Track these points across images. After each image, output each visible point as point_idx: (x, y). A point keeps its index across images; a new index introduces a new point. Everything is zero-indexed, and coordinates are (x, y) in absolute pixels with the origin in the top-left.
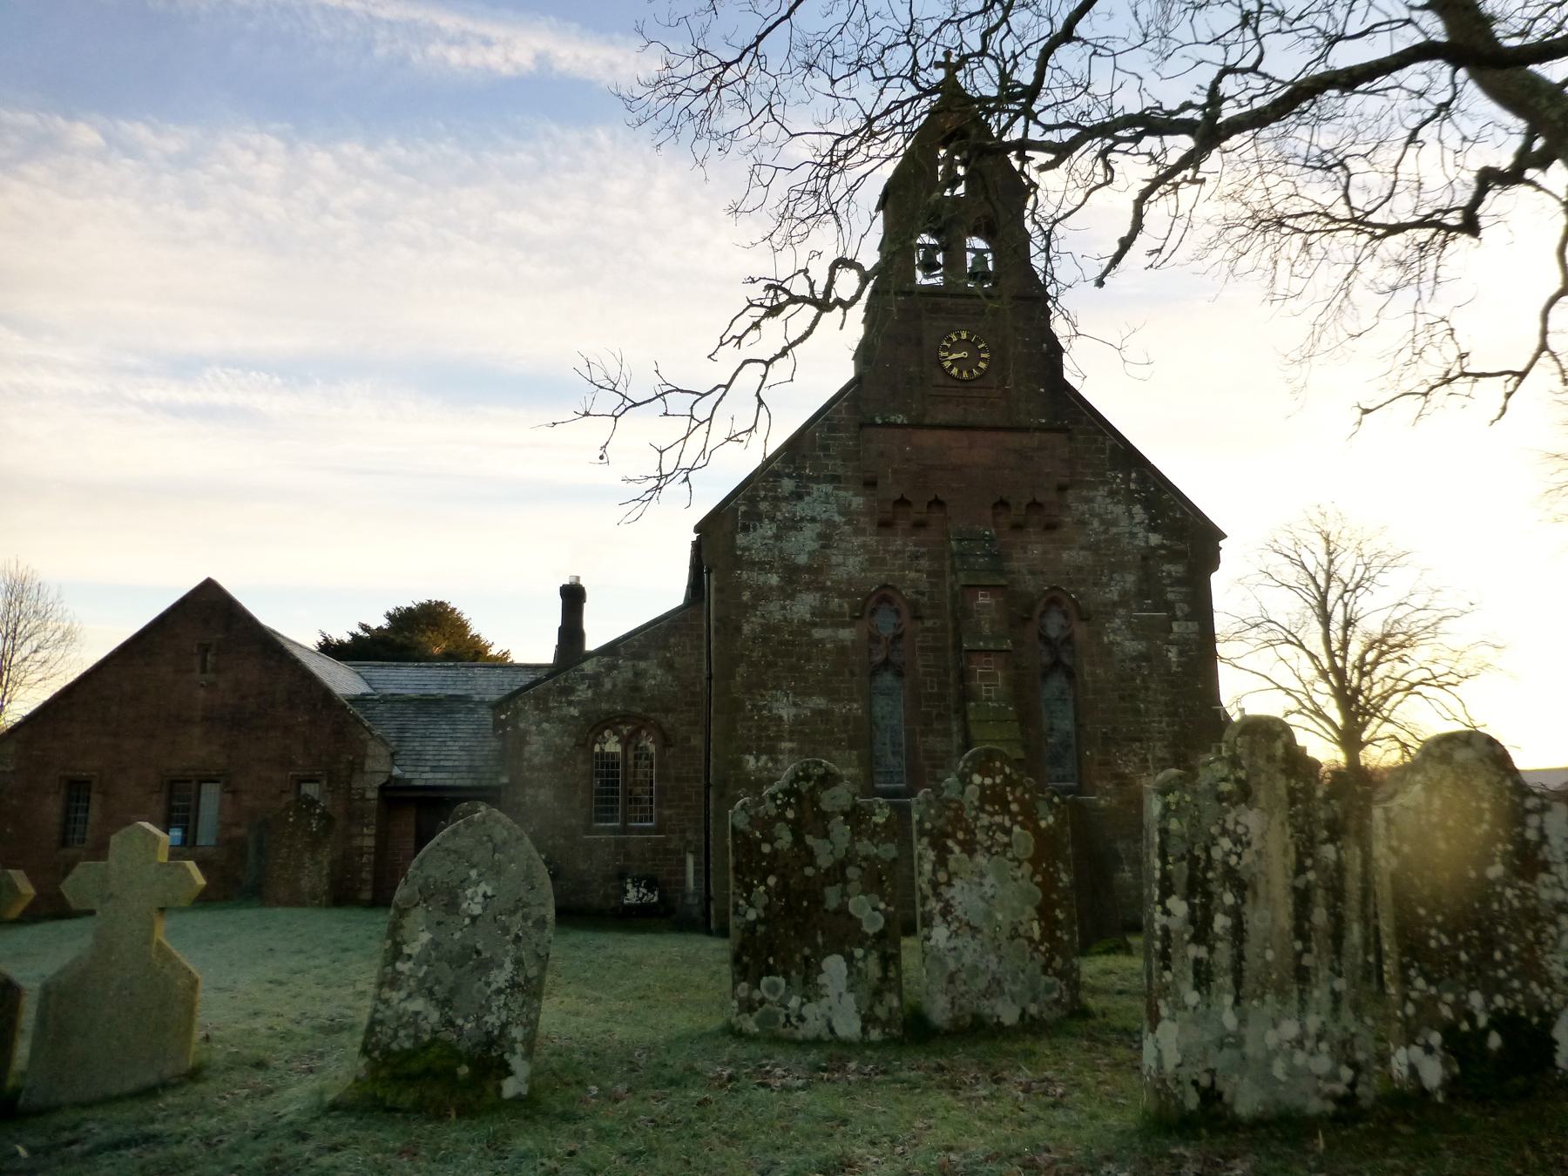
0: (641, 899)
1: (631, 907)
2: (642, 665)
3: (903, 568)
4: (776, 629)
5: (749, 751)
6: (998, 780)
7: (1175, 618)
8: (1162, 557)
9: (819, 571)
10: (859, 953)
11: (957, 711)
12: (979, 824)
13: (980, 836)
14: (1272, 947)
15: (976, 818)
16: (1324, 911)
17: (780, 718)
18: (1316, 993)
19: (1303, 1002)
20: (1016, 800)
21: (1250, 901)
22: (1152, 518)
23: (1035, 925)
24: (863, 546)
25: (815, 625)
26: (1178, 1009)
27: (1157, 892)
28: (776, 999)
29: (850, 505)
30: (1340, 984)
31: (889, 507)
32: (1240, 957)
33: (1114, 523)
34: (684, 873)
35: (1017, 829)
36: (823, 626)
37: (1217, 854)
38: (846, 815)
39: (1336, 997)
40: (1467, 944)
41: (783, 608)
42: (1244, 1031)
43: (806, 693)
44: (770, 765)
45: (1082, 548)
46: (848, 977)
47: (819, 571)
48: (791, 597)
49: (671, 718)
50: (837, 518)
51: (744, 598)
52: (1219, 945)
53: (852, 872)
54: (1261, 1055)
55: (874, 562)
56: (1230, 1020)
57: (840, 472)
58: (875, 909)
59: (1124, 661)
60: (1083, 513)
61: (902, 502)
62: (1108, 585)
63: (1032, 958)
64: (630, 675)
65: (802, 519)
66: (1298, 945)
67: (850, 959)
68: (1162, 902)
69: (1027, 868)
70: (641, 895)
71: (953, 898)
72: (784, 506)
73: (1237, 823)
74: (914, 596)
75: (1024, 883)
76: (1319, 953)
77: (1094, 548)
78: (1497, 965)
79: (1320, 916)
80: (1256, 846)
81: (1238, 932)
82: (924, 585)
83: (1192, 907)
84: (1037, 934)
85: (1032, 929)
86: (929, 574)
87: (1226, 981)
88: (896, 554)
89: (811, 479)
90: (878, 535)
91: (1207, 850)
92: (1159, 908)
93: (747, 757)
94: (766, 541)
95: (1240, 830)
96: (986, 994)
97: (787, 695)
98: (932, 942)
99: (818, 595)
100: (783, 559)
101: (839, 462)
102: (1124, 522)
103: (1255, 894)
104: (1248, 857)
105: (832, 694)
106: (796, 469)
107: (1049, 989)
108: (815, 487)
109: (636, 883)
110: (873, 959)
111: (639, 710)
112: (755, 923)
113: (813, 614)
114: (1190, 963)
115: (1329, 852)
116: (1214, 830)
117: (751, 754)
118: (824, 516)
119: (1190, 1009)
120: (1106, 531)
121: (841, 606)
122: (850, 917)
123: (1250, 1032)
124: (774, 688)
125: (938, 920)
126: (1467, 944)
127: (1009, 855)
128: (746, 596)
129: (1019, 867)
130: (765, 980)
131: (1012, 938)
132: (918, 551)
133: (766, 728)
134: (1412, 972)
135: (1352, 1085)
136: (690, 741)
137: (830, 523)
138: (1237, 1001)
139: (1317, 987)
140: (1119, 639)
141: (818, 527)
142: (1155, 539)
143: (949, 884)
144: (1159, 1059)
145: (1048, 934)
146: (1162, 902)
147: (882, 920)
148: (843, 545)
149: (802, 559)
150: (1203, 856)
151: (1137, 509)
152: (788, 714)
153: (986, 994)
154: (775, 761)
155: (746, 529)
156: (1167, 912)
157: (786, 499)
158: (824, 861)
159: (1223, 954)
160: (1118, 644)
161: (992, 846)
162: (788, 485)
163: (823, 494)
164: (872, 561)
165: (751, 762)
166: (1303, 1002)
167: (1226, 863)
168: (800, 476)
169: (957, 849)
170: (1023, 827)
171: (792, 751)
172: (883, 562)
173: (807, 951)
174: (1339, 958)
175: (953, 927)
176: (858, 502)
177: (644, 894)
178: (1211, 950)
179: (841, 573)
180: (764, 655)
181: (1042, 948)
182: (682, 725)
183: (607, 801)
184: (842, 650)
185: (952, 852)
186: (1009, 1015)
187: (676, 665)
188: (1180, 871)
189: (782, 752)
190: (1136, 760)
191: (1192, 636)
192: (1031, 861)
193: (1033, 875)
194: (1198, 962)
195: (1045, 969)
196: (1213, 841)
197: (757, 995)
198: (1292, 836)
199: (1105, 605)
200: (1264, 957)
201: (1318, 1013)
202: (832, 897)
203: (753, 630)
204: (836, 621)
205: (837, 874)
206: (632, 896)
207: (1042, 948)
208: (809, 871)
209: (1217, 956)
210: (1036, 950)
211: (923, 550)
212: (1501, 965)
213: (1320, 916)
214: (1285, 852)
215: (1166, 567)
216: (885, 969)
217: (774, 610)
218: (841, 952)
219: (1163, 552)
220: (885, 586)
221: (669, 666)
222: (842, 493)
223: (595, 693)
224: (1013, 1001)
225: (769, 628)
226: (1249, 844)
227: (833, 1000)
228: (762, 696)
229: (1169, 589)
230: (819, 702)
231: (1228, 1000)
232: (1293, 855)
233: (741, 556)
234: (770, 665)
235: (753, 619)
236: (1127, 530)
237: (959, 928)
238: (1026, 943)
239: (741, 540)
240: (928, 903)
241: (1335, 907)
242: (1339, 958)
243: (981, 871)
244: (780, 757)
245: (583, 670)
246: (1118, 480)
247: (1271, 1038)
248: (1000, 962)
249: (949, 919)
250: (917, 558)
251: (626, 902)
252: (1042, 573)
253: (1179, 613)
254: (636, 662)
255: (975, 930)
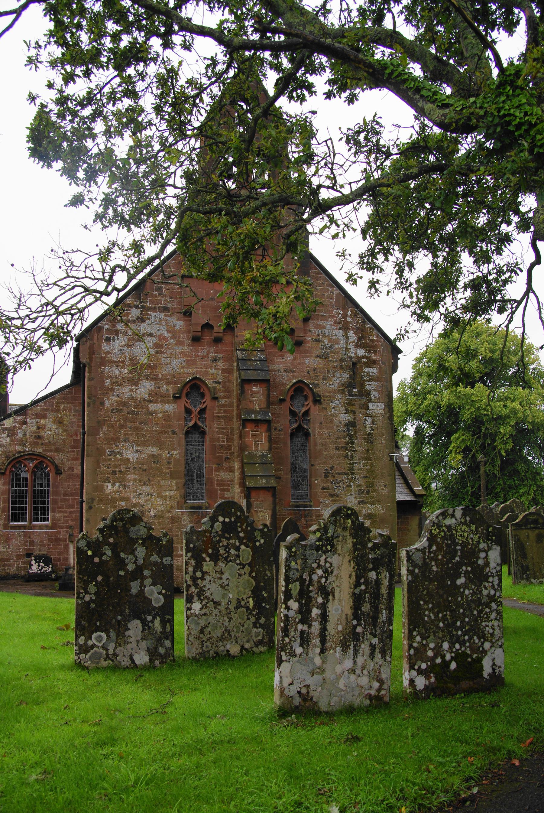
0: (40, 570)
1: (35, 575)
2: (43, 422)
3: (207, 367)
4: (126, 404)
5: (108, 480)
6: (233, 519)
7: (370, 401)
8: (364, 363)
9: (155, 367)
10: (149, 618)
11: (238, 456)
12: (221, 544)
13: (222, 552)
14: (341, 624)
15: (220, 541)
16: (369, 605)
17: (128, 460)
18: (363, 646)
19: (356, 651)
20: (243, 531)
21: (331, 601)
22: (359, 339)
23: (251, 600)
24: (182, 353)
25: (151, 401)
26: (292, 656)
27: (282, 597)
28: (101, 645)
29: (174, 326)
30: (375, 641)
31: (200, 329)
32: (323, 630)
33: (337, 341)
34: (68, 554)
35: (243, 547)
36: (156, 402)
37: (315, 577)
38: (144, 540)
39: (373, 647)
40: (444, 619)
41: (131, 391)
42: (324, 666)
43: (145, 444)
44: (121, 489)
45: (317, 357)
46: (142, 632)
47: (155, 367)
48: (136, 384)
49: (61, 456)
50: (166, 334)
51: (107, 384)
52: (314, 623)
53: (146, 573)
54: (333, 677)
55: (189, 362)
56: (318, 661)
57: (169, 305)
58: (159, 593)
59: (339, 426)
60: (319, 335)
61: (207, 326)
62: (330, 380)
63: (248, 619)
64: (34, 428)
65: (144, 335)
66: (355, 622)
67: (144, 623)
68: (285, 602)
69: (247, 569)
70: (40, 568)
71: (204, 586)
72: (133, 326)
73: (326, 562)
74: (214, 385)
75: (246, 577)
76: (365, 625)
77: (323, 356)
78: (457, 629)
79: (366, 607)
80: (335, 573)
81: (324, 618)
82: (220, 378)
83: (301, 605)
84: (251, 604)
85: (248, 602)
86: (224, 371)
87: (317, 641)
88: (203, 357)
89: (149, 309)
90: (192, 345)
91: (310, 576)
92: (284, 606)
93: (106, 484)
94: (121, 348)
95: (328, 565)
96: (222, 639)
97: (132, 445)
98: (192, 611)
99: (153, 383)
100: (131, 360)
101: (168, 299)
102: (343, 341)
103: (334, 596)
104: (330, 579)
105: (160, 445)
106: (141, 302)
107: (257, 635)
108: (153, 314)
109: (37, 561)
110: (157, 622)
111: (40, 451)
112: (89, 603)
113: (150, 395)
114: (298, 634)
115: (373, 575)
116: (314, 565)
117: (109, 482)
118: (158, 333)
119: (298, 656)
120: (332, 347)
121: (167, 390)
122: (146, 598)
123: (328, 667)
124: (125, 441)
125: (196, 598)
126: (444, 619)
127: (238, 562)
128: (107, 383)
129: (243, 568)
130: (94, 635)
131: (237, 608)
132: (216, 356)
133: (119, 466)
134: (415, 633)
135: (379, 690)
136: (73, 471)
137: (161, 337)
138: (322, 651)
139: (363, 642)
140: (337, 413)
141: (155, 340)
142: (361, 352)
143: (202, 578)
144: (281, 682)
145: (257, 604)
146: (285, 602)
147: (163, 600)
148: (169, 351)
149: (144, 360)
150: (308, 579)
151: (351, 334)
152: (133, 458)
153: (222, 639)
154: (125, 487)
155: (108, 340)
156: (288, 608)
157: (134, 321)
158: (131, 567)
159: (316, 627)
160: (336, 416)
161: (228, 556)
162: (135, 313)
163: (157, 319)
164: (187, 362)
165: (109, 487)
166: (356, 651)
167: (319, 582)
168: (143, 307)
169: (208, 559)
170: (247, 546)
171: (135, 480)
172: (194, 362)
173: (119, 618)
174: (375, 628)
175: (204, 603)
176: (180, 324)
177: (43, 567)
178: (310, 626)
179: (167, 369)
180: (118, 420)
181: (254, 613)
182: (68, 460)
183: (19, 508)
184: (167, 417)
185: (206, 561)
186: (234, 649)
187: (65, 422)
188: (295, 588)
189: (129, 481)
190: (344, 486)
191: (380, 412)
192: (249, 564)
193: (250, 573)
194: (302, 632)
195: (255, 626)
196: (312, 571)
197: (90, 643)
198: (354, 568)
199: (330, 392)
200: (337, 629)
201: (363, 656)
202: (135, 588)
203: (112, 404)
204: (162, 398)
205: (137, 574)
206: (34, 569)
207: (254, 613)
208: (122, 573)
209: (313, 629)
210: (251, 613)
211: (221, 355)
212: (460, 628)
213: (366, 607)
214: (350, 576)
215: (367, 370)
216: (164, 627)
217: (125, 391)
218: (139, 618)
219: (365, 360)
220: (196, 378)
221: (59, 422)
222: (169, 319)
223: (12, 440)
224: (237, 642)
225: (122, 404)
226: (332, 572)
227: (134, 645)
228: (117, 446)
229: (368, 383)
230: (153, 450)
231: (318, 650)
232: (354, 577)
233: (105, 357)
234: (122, 427)
235: (112, 398)
236: (345, 346)
237: (207, 603)
238: (245, 610)
239: (105, 347)
240: (190, 589)
241: (374, 603)
242: (375, 628)
243: (221, 571)
244: (128, 484)
245: (4, 425)
246: (340, 315)
247: (339, 669)
248: (230, 621)
249: (202, 598)
250: (216, 360)
251: (31, 572)
252: (293, 371)
253: (373, 398)
254: (38, 420)
255: (217, 604)
